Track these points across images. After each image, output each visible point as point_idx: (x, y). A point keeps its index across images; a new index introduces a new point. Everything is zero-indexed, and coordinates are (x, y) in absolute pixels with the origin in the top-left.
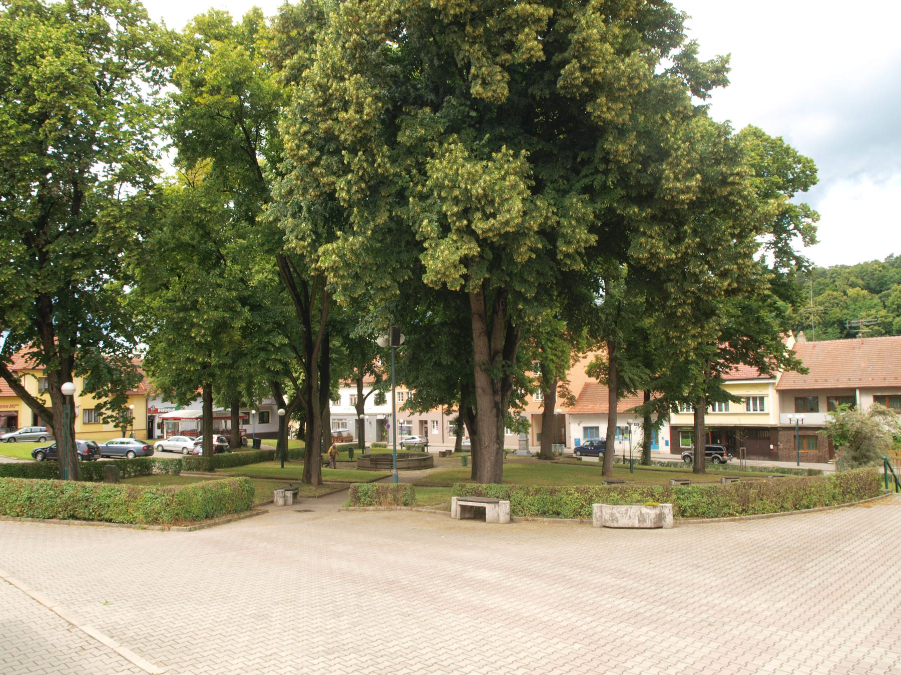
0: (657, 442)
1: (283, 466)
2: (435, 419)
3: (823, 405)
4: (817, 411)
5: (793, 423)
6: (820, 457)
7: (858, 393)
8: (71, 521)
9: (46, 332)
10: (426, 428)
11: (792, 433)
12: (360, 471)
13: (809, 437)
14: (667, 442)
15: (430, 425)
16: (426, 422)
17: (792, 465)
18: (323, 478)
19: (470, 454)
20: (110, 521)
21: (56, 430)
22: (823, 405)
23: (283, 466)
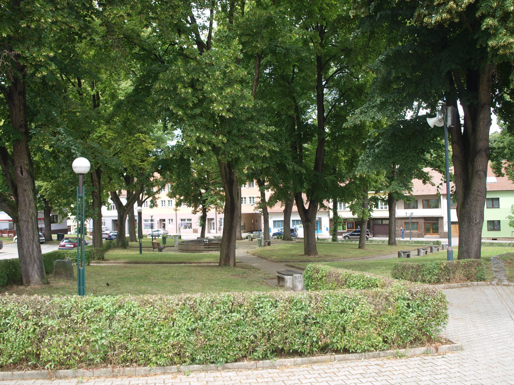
0: (321, 228)
1: (141, 253)
2: (171, 218)
3: (420, 205)
4: (417, 208)
5: (408, 215)
6: (419, 234)
7: (442, 197)
8: (279, 361)
9: (16, 102)
10: (164, 224)
11: (404, 221)
12: (181, 253)
13: (413, 223)
14: (327, 229)
15: (167, 222)
16: (164, 220)
17: (408, 239)
18: (236, 261)
19: (91, 241)
20: (346, 351)
21: (21, 223)
22: (420, 205)
23: (141, 253)
